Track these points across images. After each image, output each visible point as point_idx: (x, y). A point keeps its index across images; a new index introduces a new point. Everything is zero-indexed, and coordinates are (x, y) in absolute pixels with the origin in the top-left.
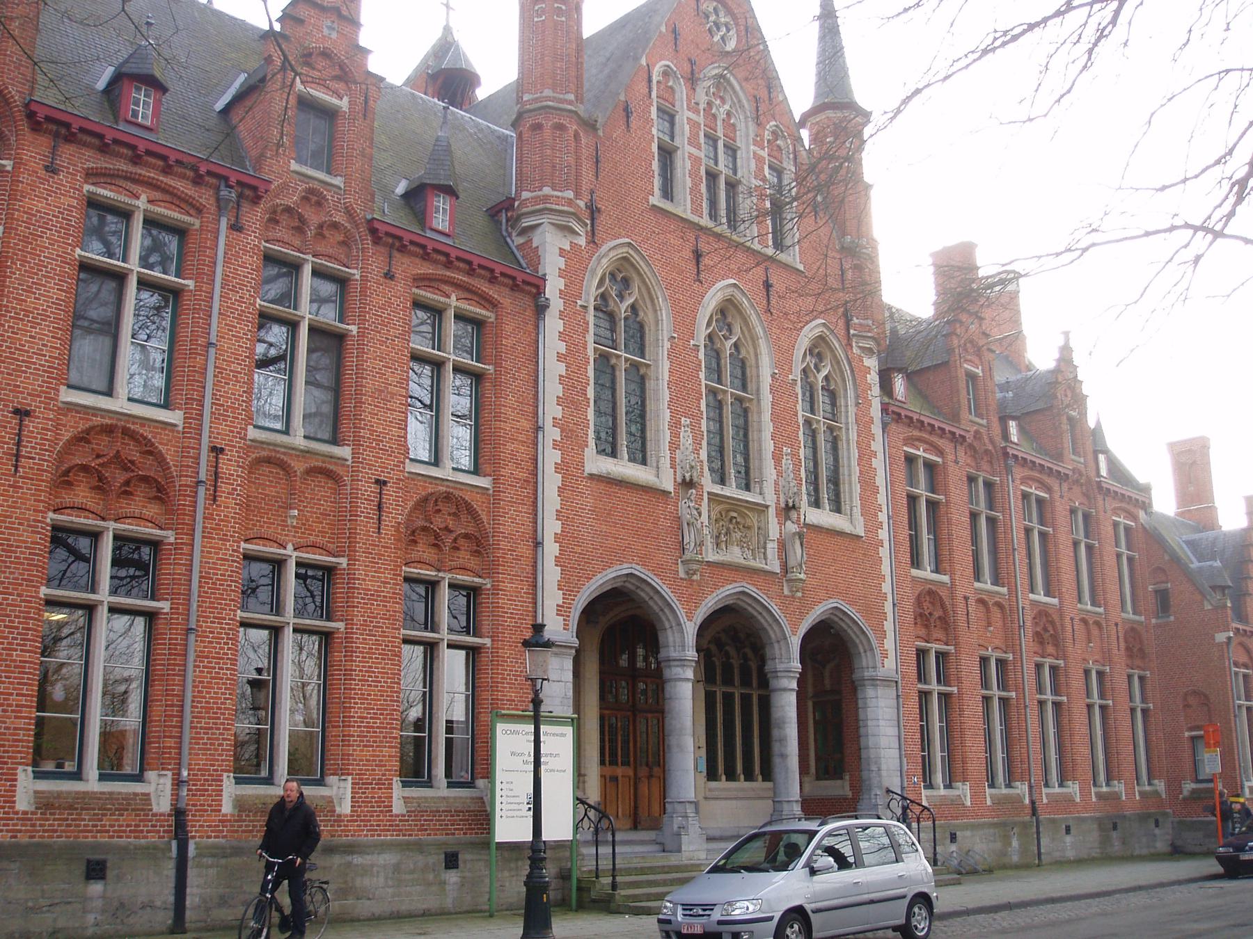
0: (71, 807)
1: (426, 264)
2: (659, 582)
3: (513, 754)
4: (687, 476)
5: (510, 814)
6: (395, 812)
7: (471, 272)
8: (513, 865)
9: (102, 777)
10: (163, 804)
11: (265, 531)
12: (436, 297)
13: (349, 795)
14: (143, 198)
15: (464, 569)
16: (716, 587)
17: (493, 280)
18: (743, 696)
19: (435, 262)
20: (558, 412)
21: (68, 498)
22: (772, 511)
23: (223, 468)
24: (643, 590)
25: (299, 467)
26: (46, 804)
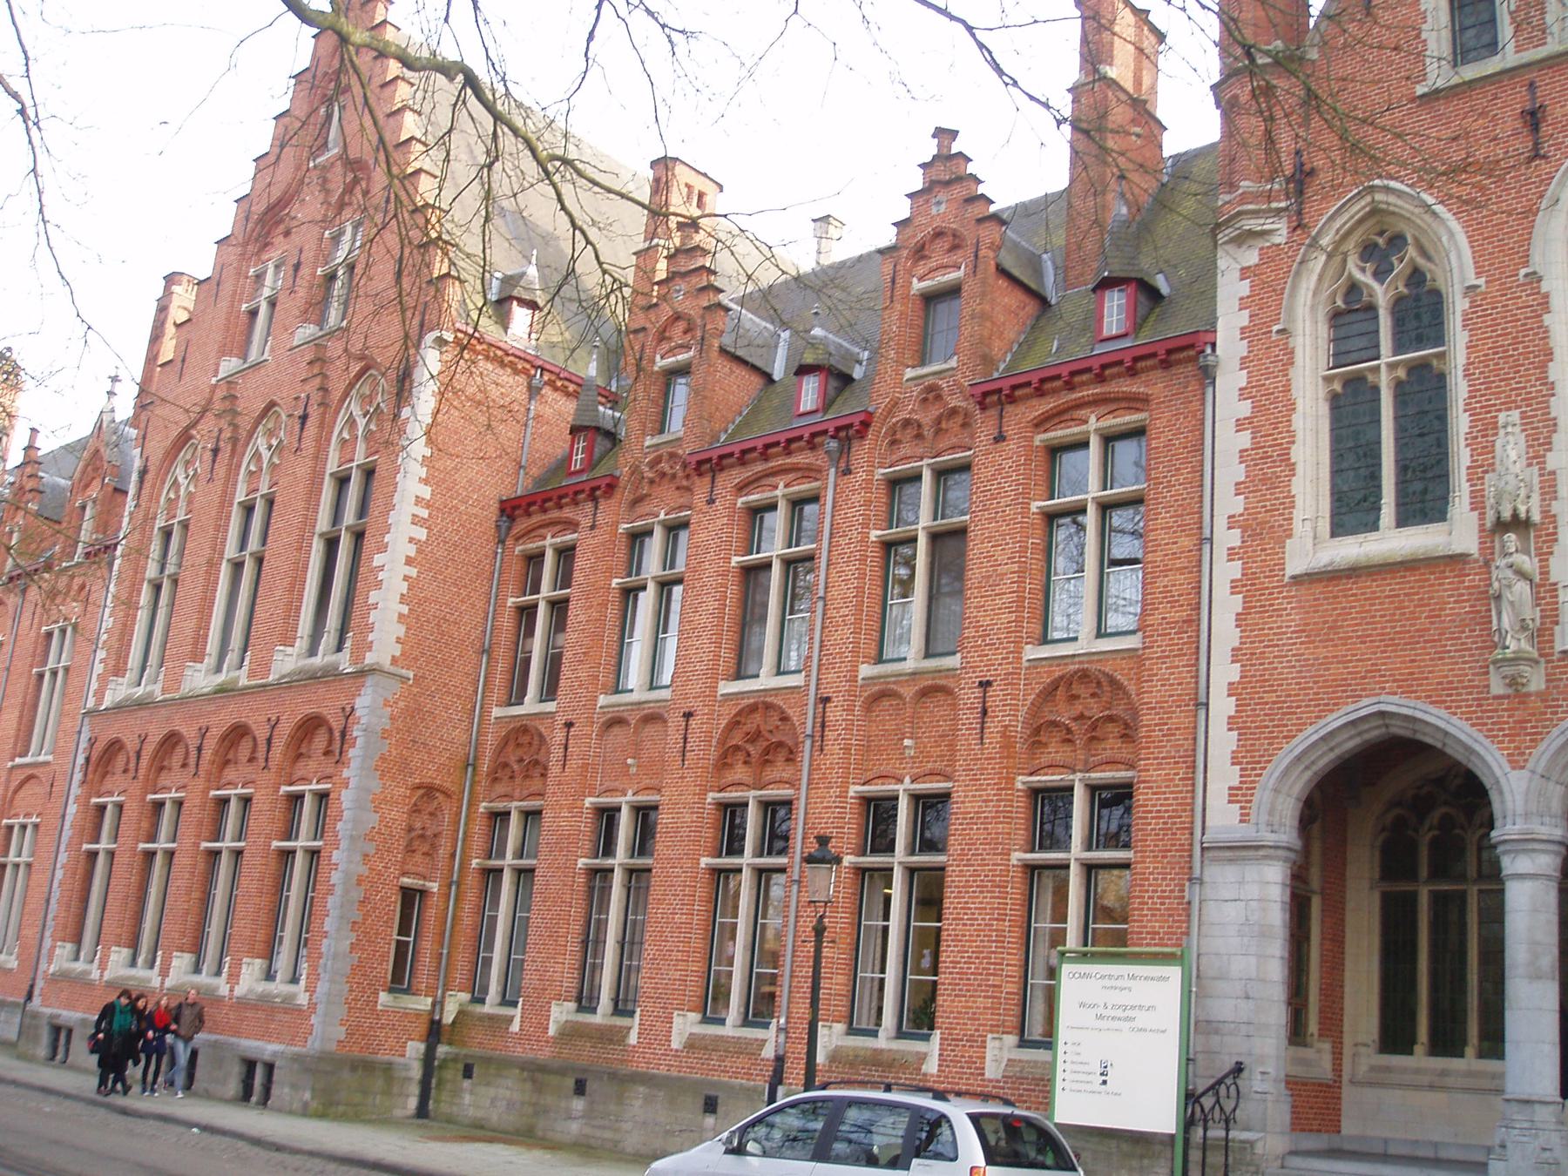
0: (706, 1048)
1: (1043, 400)
3: (1082, 1005)
4: (1522, 509)
5: (1076, 1086)
6: (988, 1075)
7: (1101, 379)
8: (1134, 1163)
9: (900, 1034)
10: (769, 1052)
11: (883, 769)
12: (1068, 431)
13: (937, 1053)
14: (1093, 419)
15: (1111, 762)
17: (1132, 372)
18: (1438, 900)
19: (1055, 391)
20: (1237, 505)
21: (731, 777)
23: (830, 716)
25: (908, 692)
26: (693, 1044)
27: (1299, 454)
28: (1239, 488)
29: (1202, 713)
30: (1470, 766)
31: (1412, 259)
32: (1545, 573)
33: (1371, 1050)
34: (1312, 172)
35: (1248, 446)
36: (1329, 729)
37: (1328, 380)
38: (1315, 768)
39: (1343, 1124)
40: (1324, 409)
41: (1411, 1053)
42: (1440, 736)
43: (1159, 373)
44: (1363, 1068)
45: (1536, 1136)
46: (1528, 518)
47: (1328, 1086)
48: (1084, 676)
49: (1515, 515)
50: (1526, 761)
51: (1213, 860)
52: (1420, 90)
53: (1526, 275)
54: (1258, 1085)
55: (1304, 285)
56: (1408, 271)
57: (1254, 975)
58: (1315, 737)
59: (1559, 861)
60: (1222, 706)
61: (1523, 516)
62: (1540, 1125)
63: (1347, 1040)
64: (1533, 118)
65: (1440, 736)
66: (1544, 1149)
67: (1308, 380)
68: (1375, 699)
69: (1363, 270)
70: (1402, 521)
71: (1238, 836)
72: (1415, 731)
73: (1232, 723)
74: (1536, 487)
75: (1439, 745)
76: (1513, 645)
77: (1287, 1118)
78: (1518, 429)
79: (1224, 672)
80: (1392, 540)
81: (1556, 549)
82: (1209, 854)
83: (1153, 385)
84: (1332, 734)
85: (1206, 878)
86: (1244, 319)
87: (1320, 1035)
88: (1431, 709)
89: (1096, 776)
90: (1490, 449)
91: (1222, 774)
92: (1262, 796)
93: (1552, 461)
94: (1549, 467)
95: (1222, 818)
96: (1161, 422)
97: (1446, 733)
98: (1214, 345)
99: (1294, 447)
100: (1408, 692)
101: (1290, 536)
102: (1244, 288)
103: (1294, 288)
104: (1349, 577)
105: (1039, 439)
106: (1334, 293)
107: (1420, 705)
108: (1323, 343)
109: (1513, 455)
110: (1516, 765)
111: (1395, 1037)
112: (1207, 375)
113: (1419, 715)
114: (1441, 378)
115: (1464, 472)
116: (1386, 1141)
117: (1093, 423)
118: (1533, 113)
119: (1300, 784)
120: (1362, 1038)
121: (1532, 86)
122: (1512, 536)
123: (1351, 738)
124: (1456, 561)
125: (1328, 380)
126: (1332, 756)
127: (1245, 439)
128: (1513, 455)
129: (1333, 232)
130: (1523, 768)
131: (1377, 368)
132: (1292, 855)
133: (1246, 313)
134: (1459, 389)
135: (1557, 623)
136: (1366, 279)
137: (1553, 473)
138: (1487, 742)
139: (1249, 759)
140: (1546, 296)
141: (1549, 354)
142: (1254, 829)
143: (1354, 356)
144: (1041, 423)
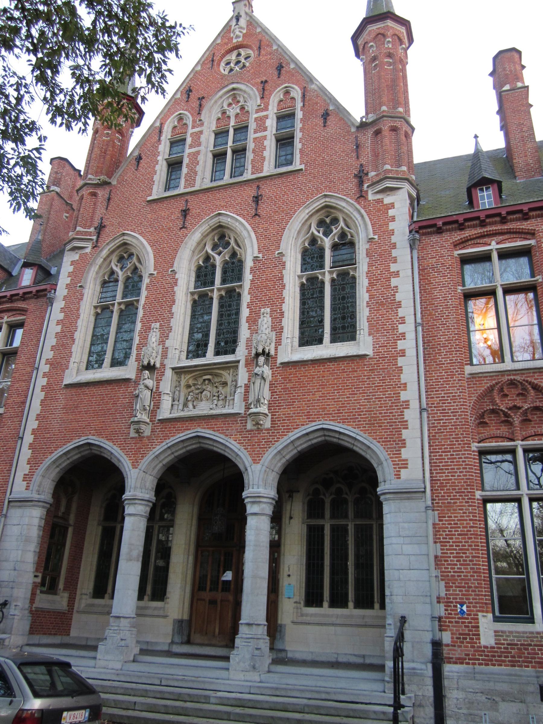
14: (6, 317)
16: (166, 437)
27: (77, 335)
28: (53, 348)
29: (19, 442)
30: (236, 462)
31: (342, 228)
32: (158, 388)
33: (88, 597)
34: (104, 227)
35: (59, 331)
36: (67, 449)
37: (300, 277)
38: (61, 467)
39: (71, 631)
40: (298, 290)
41: (103, 597)
42: (109, 454)
43: (33, 300)
44: (83, 605)
45: (119, 633)
46: (154, 365)
47: (64, 613)
48: (512, 383)
49: (149, 364)
50: (260, 460)
51: (12, 507)
52: (149, 198)
53: (278, 254)
54: (12, 612)
55: (93, 269)
56: (133, 268)
57: (19, 560)
58: (61, 453)
59: (148, 509)
60: (28, 438)
61: (152, 364)
62: (122, 628)
63: (78, 592)
64: (185, 213)
65: (109, 454)
66: (122, 640)
67: (87, 307)
68: (86, 438)
69: (117, 266)
70: (333, 340)
71: (23, 496)
72: (101, 452)
73: (31, 446)
74: (274, 341)
75: (109, 458)
76: (138, 415)
77: (28, 628)
78: (157, 330)
79: (32, 424)
80: (328, 349)
81: (163, 378)
82: (11, 504)
83: (30, 305)
84: (68, 452)
85: (8, 515)
86: (68, 280)
87: (64, 590)
88: (107, 442)
89: (530, 443)
90: (146, 338)
91: (23, 468)
92: (37, 478)
93: (168, 343)
94: (166, 346)
95: (19, 488)
96: (29, 319)
97: (112, 453)
98: (55, 290)
99: (76, 333)
100: (99, 435)
101: (67, 369)
102: (71, 269)
103: (89, 270)
104: (86, 386)
105: (456, 253)
106: (104, 274)
107: (102, 440)
108: (97, 293)
109: (154, 340)
110: (134, 467)
111: (313, 598)
112: (51, 302)
113: (102, 444)
114: (239, 295)
115: (136, 346)
116: (87, 639)
117: (6, 319)
118: (256, 197)
119: (54, 474)
120: (84, 591)
121: (187, 201)
122: (147, 372)
123: (76, 454)
124: (127, 380)
125: (300, 277)
126: (68, 462)
127: (59, 328)
128: (154, 340)
129: (107, 250)
130: (136, 468)
131: (114, 304)
132: (48, 506)
133: (70, 278)
134: (246, 298)
135: (159, 408)
136: (117, 269)
137: (167, 348)
138: (125, 457)
139: (34, 462)
140: (177, 280)
141: (174, 302)
142: (30, 492)
143: (108, 299)
144: (457, 245)
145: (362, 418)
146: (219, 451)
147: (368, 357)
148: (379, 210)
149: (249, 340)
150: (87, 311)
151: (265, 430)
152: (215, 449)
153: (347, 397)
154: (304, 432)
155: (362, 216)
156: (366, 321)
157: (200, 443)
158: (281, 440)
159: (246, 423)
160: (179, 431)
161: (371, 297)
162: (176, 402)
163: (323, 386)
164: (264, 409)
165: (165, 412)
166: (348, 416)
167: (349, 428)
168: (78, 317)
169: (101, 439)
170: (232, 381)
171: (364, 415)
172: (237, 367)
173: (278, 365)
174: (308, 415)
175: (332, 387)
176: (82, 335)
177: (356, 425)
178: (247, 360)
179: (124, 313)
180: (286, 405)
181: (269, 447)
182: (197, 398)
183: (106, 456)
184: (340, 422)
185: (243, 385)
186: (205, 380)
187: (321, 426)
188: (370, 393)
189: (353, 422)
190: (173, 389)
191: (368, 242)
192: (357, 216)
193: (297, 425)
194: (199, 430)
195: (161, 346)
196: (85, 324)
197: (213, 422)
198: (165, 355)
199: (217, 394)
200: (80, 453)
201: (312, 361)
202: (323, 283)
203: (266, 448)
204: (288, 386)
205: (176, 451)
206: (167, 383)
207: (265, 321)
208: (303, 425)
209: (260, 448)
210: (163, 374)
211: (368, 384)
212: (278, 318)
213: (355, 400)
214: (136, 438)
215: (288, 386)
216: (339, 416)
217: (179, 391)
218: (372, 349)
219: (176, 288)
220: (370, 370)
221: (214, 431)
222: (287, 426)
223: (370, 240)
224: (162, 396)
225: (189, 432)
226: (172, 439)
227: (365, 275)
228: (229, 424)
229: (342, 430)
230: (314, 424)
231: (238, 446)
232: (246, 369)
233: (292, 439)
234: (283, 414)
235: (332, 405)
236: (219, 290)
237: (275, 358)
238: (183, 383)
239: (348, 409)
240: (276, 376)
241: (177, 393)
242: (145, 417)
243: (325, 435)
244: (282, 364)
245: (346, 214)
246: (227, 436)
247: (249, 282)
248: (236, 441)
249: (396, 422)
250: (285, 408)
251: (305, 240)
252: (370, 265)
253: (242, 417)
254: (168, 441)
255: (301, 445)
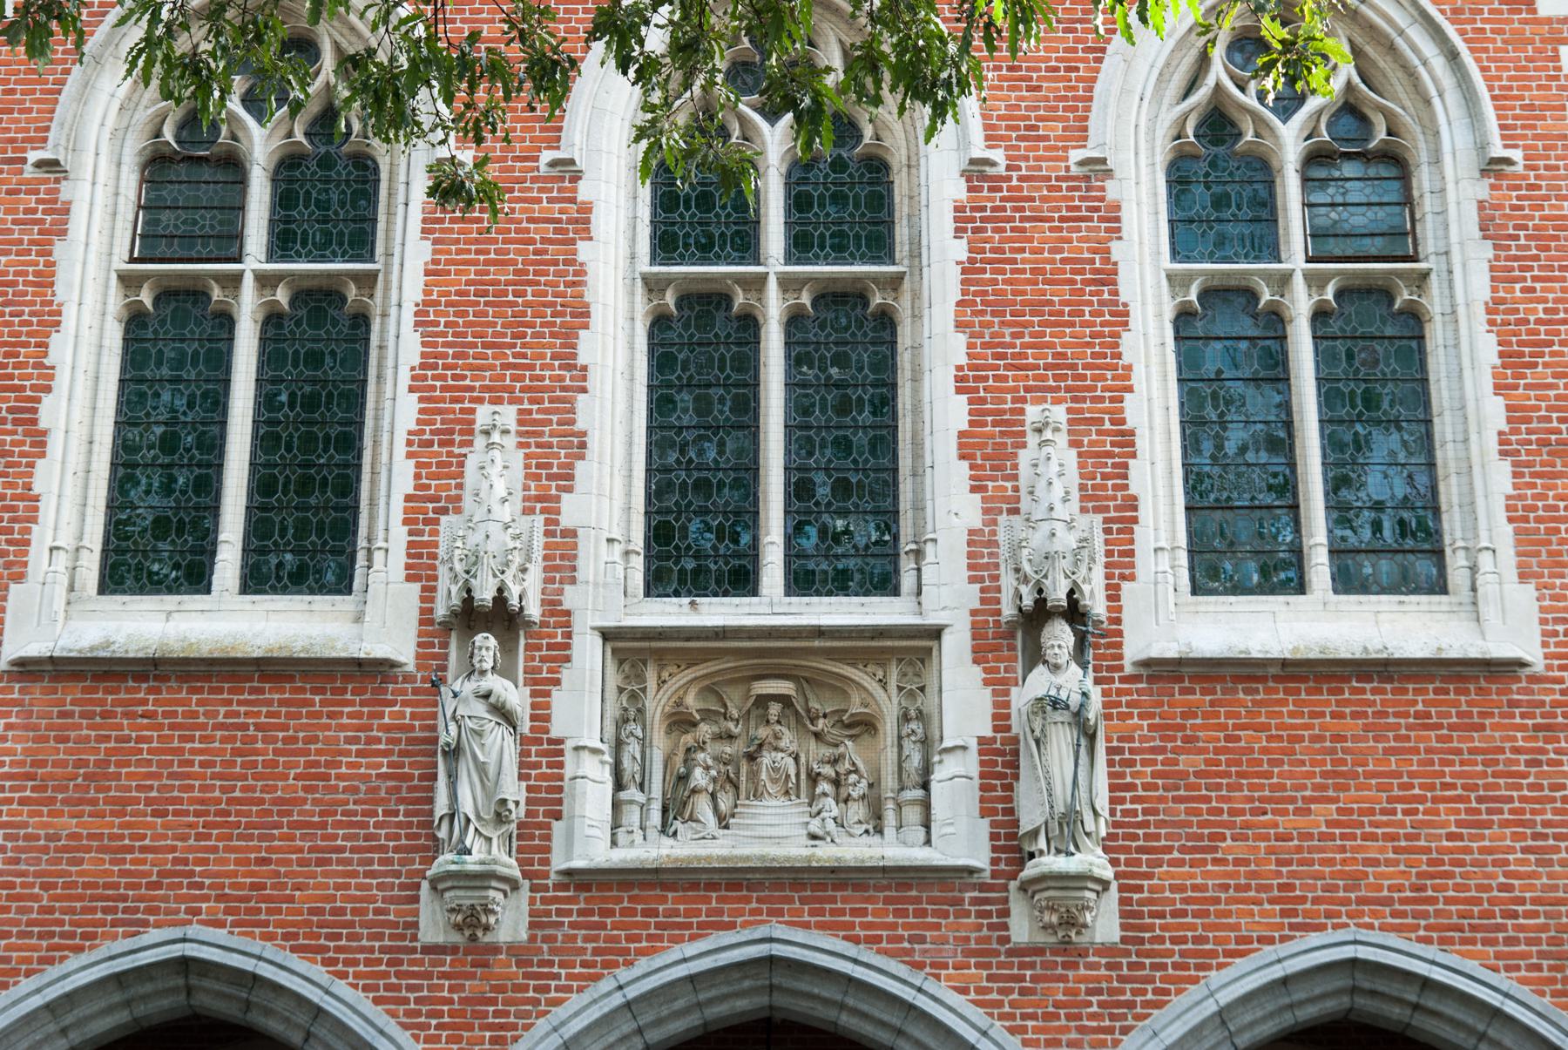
2: (318, 972)
16: (614, 957)
22: (956, 647)
24: (268, 1012)
40: (114, 336)
53: (553, 164)
58: (36, 1001)
68: (176, 933)
81: (565, 674)
84: (70, 998)
93: (571, 510)
94: (566, 521)
99: (47, 400)
101: (19, 577)
107: (269, 950)
123: (109, 1010)
125: (129, 282)
134: (399, 347)
135: (558, 816)
140: (586, 209)
141: (582, 314)
145: (1521, 928)
146: (867, 1029)
147: (1527, 671)
148: (1520, 41)
149: (980, 545)
150: (92, 298)
151: (1098, 953)
152: (846, 1020)
153: (1451, 837)
154: (1277, 972)
155: (1453, 56)
156: (1502, 515)
157: (772, 988)
158: (1178, 1002)
159: (1006, 913)
160: (679, 931)
161: (1517, 415)
162: (633, 793)
163: (1340, 777)
164: (1091, 860)
165: (590, 838)
166: (1462, 916)
167: (1471, 966)
168: (51, 319)
169: (256, 947)
170: (905, 718)
171: (1527, 915)
172: (925, 656)
173: (1128, 670)
174: (1287, 899)
175: (1380, 787)
176: (79, 412)
177: (1498, 956)
178: (977, 632)
179: (1199, 328)
180: (1182, 849)
181: (1125, 1031)
182: (738, 781)
183: (274, 1026)
184: (1427, 941)
185: (973, 745)
186: (763, 701)
187: (1347, 952)
188: (1546, 824)
189: (1485, 942)
190: (610, 729)
191: (1484, 173)
192: (1429, 49)
193: (1239, 940)
194: (780, 931)
195: (539, 520)
196: (86, 359)
197: (843, 901)
198: (562, 557)
199: (828, 770)
200: (127, 1004)
201: (1284, 663)
202: (226, 321)
203: (1110, 1030)
204: (1185, 762)
205: (658, 1022)
206: (583, 703)
207: (1054, 468)
208: (1270, 941)
209: (1082, 1030)
210: (561, 654)
211: (1531, 787)
212: (1107, 455)
213: (1482, 850)
214: (454, 949)
215: (1185, 762)
216: (1425, 915)
217: (644, 742)
218: (1538, 639)
219: (59, 249)
220: (1537, 728)
221: (856, 940)
222: (1198, 940)
223: (1493, 168)
224: (569, 758)
225: (728, 938)
226: (643, 965)
227: (1481, 316)
228: (922, 913)
229: (1438, 975)
230: (1315, 939)
231: (977, 1015)
232: (977, 672)
233: (1225, 997)
234: (1173, 889)
235: (1388, 862)
236: (265, 281)
237: (1114, 633)
238: (656, 704)
239: (1457, 888)
240: (1123, 717)
241: (633, 748)
242: (488, 851)
243: (1354, 990)
244: (1147, 663)
245: (1371, 28)
246: (919, 966)
247: (955, 274)
248: (963, 991)
249: (368, 874)
250: (1181, 863)
251: (1184, 118)
252: (1500, 276)
253: (983, 887)
254: (624, 974)
255: (1252, 1025)
